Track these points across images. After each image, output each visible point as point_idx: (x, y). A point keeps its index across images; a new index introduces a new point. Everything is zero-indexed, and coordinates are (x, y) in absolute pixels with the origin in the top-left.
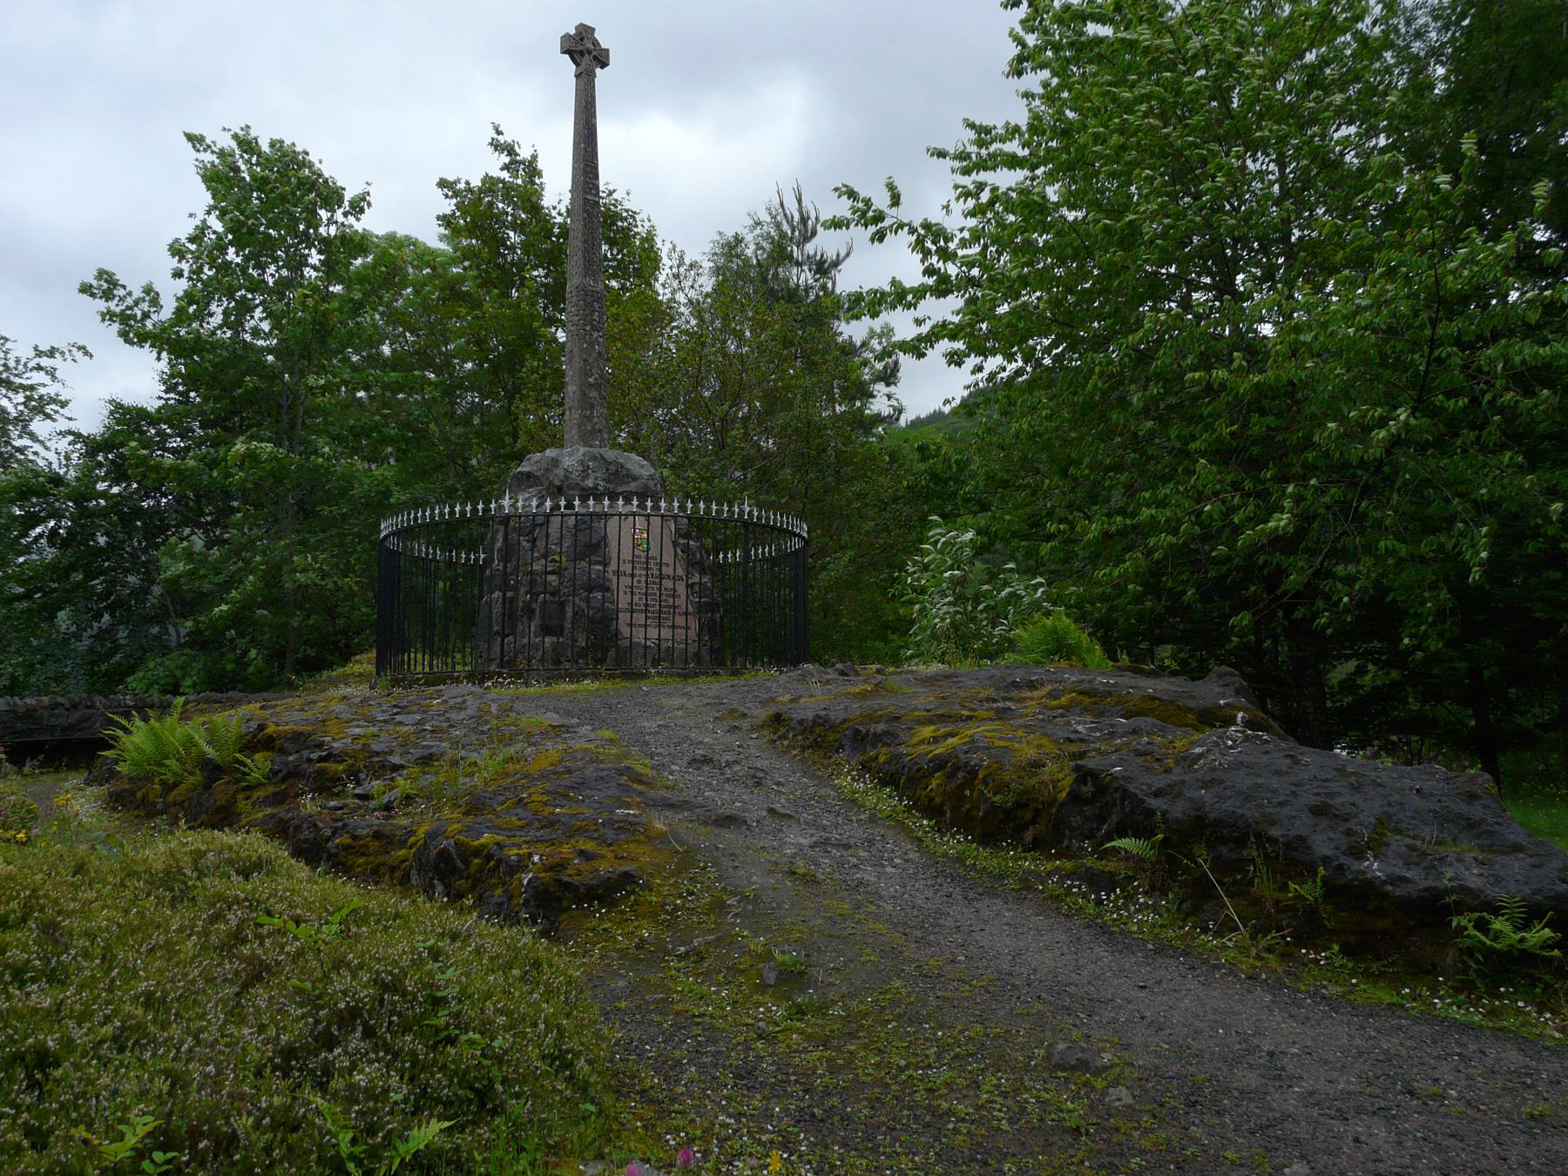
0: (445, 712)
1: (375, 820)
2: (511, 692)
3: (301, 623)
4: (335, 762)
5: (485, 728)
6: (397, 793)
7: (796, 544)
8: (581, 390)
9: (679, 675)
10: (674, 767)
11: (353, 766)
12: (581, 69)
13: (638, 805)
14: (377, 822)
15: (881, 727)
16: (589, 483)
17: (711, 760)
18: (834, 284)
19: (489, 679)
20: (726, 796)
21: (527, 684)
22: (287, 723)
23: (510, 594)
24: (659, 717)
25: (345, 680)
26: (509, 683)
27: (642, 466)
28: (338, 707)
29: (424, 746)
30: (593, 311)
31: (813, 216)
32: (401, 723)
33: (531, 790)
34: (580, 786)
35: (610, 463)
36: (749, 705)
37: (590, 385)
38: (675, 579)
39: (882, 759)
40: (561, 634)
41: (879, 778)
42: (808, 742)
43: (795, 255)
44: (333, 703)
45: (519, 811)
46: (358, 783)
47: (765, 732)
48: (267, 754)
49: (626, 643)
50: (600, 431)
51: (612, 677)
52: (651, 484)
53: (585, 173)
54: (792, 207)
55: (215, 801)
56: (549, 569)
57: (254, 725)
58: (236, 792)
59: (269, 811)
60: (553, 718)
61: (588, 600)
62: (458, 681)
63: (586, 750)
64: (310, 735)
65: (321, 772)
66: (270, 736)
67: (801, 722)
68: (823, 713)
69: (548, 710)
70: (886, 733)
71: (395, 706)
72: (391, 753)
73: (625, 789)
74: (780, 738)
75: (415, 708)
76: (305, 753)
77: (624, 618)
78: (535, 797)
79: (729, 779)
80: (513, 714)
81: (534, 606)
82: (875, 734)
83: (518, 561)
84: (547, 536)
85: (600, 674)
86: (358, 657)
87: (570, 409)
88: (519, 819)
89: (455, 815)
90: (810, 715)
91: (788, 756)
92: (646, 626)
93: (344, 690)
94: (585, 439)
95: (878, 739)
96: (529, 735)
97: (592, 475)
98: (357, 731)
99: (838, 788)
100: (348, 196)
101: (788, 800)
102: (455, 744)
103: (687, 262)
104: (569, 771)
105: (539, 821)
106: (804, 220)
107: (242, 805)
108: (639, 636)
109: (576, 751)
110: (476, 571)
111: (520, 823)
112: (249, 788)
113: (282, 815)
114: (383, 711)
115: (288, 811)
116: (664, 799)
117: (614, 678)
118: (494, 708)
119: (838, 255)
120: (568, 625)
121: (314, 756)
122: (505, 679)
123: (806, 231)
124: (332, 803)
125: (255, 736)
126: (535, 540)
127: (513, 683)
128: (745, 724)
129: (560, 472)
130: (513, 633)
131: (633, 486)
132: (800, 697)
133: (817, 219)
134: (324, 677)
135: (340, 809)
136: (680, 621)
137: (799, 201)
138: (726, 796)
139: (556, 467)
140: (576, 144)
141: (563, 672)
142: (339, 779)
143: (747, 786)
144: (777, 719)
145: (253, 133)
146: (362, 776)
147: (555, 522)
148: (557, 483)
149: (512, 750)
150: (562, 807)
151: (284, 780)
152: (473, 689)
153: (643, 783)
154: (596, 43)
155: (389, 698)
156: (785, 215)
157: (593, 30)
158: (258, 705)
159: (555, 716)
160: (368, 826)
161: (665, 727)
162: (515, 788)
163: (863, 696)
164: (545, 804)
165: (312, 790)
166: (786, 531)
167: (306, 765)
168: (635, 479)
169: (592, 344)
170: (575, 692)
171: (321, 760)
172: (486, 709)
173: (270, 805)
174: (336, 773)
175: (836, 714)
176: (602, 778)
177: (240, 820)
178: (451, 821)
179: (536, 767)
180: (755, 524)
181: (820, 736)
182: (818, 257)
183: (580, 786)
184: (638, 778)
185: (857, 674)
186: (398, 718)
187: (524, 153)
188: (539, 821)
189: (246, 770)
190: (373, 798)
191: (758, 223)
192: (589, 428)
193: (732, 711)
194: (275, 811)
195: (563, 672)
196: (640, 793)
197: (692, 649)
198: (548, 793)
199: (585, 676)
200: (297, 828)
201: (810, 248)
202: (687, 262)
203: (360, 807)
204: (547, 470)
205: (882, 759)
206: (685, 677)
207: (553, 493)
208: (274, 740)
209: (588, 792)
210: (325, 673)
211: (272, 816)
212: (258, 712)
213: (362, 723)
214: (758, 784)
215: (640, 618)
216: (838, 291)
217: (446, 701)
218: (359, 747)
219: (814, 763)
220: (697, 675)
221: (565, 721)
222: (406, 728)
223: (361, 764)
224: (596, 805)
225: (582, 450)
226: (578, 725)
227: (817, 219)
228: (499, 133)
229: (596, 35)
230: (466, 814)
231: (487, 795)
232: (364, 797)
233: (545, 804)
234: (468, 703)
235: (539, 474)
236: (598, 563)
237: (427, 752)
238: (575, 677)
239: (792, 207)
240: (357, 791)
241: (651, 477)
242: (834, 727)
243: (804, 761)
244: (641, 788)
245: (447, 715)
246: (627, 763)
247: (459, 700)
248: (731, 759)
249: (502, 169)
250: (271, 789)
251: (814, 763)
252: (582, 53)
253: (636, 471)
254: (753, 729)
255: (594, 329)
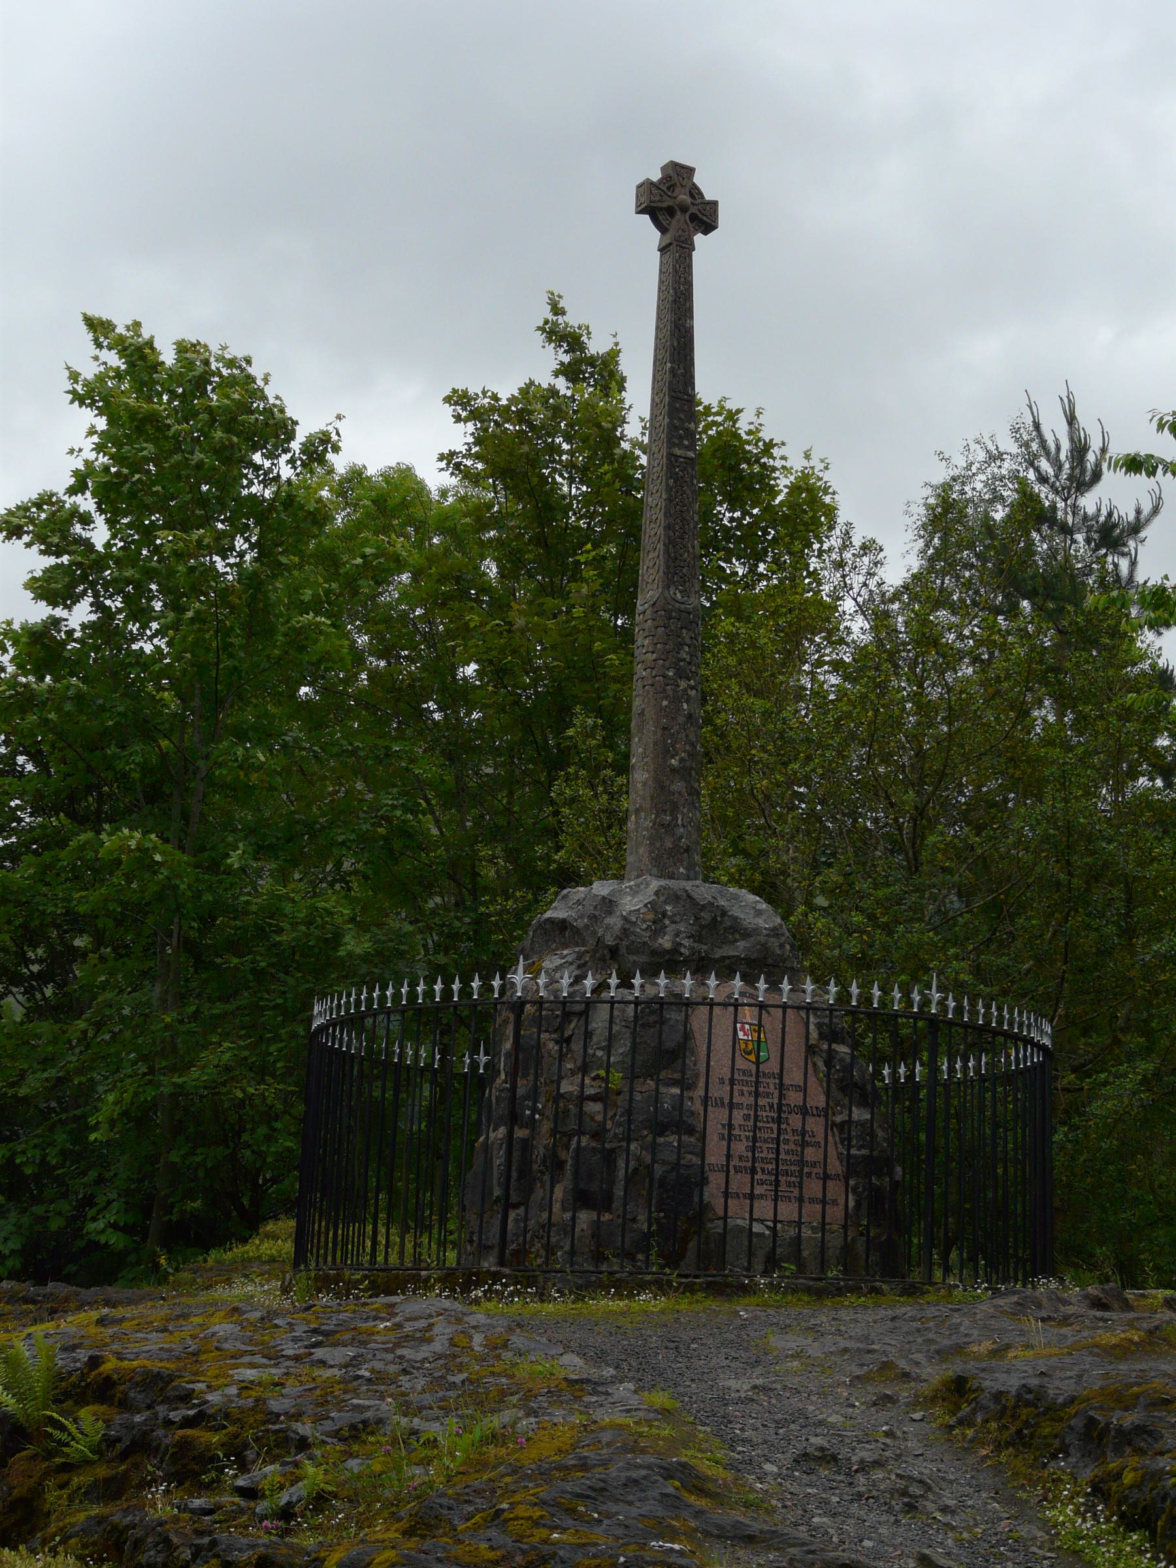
0: (397, 1345)
1: (262, 1537)
2: (513, 1309)
3: (184, 1157)
4: (211, 1429)
5: (458, 1378)
6: (300, 1490)
7: (1017, 1058)
8: (657, 780)
9: (808, 1290)
10: (768, 1467)
11: (236, 1436)
12: (668, 239)
13: (690, 1535)
14: (265, 1539)
15: (1130, 1419)
16: (665, 942)
17: (834, 1458)
18: (1133, 564)
19: (478, 1284)
20: (850, 1527)
21: (542, 1297)
22: (137, 1355)
23: (520, 1133)
24: (759, 1370)
25: (244, 1267)
26: (512, 1294)
27: (759, 913)
28: (223, 1328)
29: (356, 1408)
30: (682, 645)
31: (1095, 444)
32: (323, 1363)
33: (518, 1497)
34: (599, 1493)
35: (703, 908)
36: (917, 1357)
37: (674, 770)
38: (804, 1111)
39: (1128, 1478)
40: (608, 1209)
41: (1122, 1516)
42: (1006, 1435)
43: (1060, 514)
44: (215, 1319)
45: (492, 1533)
46: (243, 1467)
47: (938, 1410)
48: (101, 1408)
49: (717, 1227)
50: (687, 850)
51: (690, 1289)
52: (774, 943)
53: (672, 412)
54: (1055, 428)
55: (11, 1488)
56: (589, 1091)
57: (83, 1355)
58: (46, 1474)
59: (95, 1510)
60: (573, 1364)
61: (653, 1148)
62: (426, 1285)
63: (621, 1427)
64: (171, 1378)
65: (184, 1445)
66: (108, 1378)
67: (998, 1396)
68: (1034, 1382)
69: (567, 1349)
70: (1140, 1430)
71: (315, 1331)
72: (297, 1416)
73: (672, 1502)
74: (961, 1422)
75: (348, 1336)
76: (161, 1410)
77: (716, 1181)
78: (522, 1511)
79: (860, 1495)
80: (507, 1355)
81: (563, 1155)
82: (1120, 1431)
83: (536, 1076)
84: (588, 1035)
85: (669, 1283)
86: (270, 1227)
87: (637, 811)
88: (492, 1548)
89: (391, 1535)
90: (1013, 1383)
91: (971, 1460)
92: (752, 1197)
93: (241, 1289)
94: (662, 865)
95: (1128, 1439)
96: (530, 1395)
97: (671, 928)
98: (250, 1374)
99: (1048, 1526)
100: (301, 435)
101: (959, 1542)
102: (406, 1408)
103: (857, 541)
104: (584, 1466)
105: (524, 1552)
106: (1079, 450)
107: (53, 1497)
108: (739, 1220)
109: (603, 1429)
110: (479, 1082)
111: (492, 1555)
112: (67, 1468)
113: (115, 1519)
114: (295, 1340)
115: (126, 1511)
116: (737, 1524)
117: (693, 1292)
118: (478, 1339)
119: (1138, 512)
120: (619, 1192)
121: (176, 1416)
122: (505, 1286)
123: (1083, 471)
124: (197, 1503)
125: (83, 1377)
126: (568, 1041)
127: (516, 1293)
128: (904, 1393)
129: (614, 921)
130: (525, 1202)
131: (741, 948)
132: (1008, 1347)
133: (1104, 450)
134: (211, 1262)
135: (210, 1512)
136: (813, 1188)
137: (1071, 420)
138: (850, 1527)
139: (610, 913)
140: (658, 362)
141: (604, 1276)
142: (214, 1459)
143: (890, 1511)
144: (959, 1387)
145: (146, 334)
146: (250, 1454)
147: (601, 1016)
148: (609, 941)
149: (495, 1422)
150: (564, 1530)
151: (124, 1456)
152: (447, 1304)
153: (701, 1492)
154: (695, 192)
155: (308, 1315)
156: (1043, 443)
157: (691, 171)
158: (94, 1315)
159: (577, 1361)
160: (253, 1547)
161: (765, 1389)
162: (493, 1491)
163: (1123, 1351)
164: (536, 1523)
165: (168, 1478)
166: (1008, 1035)
167: (160, 1432)
168: (746, 934)
169: (676, 700)
170: (623, 1314)
171: (188, 1423)
172: (465, 1342)
173: (98, 1500)
174: (208, 1447)
175: (1060, 1388)
176: (635, 1481)
177: (47, 1525)
178: (382, 1545)
179: (534, 1454)
180: (951, 1023)
181: (1027, 1424)
182: (1102, 519)
183: (599, 1493)
184: (697, 1484)
185: (1127, 1306)
186: (319, 1353)
187: (597, 346)
188: (524, 1552)
189: (64, 1437)
190: (263, 1497)
191: (995, 457)
192: (669, 844)
193: (886, 1366)
194: (106, 1511)
195: (604, 1276)
196: (698, 1514)
197: (835, 1242)
198: (543, 1503)
199: (643, 1287)
200: (138, 1544)
201: (1088, 502)
202: (857, 541)
203: (242, 1511)
204: (593, 918)
205: (1128, 1478)
206: (819, 1294)
207: (603, 959)
208: (114, 1384)
209: (613, 1508)
210: (214, 1255)
211: (100, 1520)
212: (93, 1330)
213: (259, 1359)
214: (910, 1508)
215: (740, 1183)
216: (1140, 578)
217: (399, 1326)
218: (250, 1402)
219: (1016, 1474)
220: (840, 1292)
221: (593, 1373)
222: (327, 1373)
223: (249, 1434)
224: (620, 1531)
225: (655, 884)
226: (615, 1380)
227: (1104, 450)
228: (557, 310)
229: (697, 179)
230: (408, 1533)
231: (444, 1501)
232: (250, 1493)
233: (536, 1523)
234: (437, 1330)
235: (579, 924)
236: (675, 1083)
237: (357, 1418)
238: (625, 1287)
239: (1055, 428)
240: (240, 1482)
241: (775, 932)
242: (1052, 1411)
243: (997, 1469)
244: (702, 1503)
245: (399, 1352)
246: (685, 1456)
247: (422, 1323)
248: (868, 1456)
249: (556, 374)
250: (102, 1471)
251: (1016, 1474)
252: (671, 211)
253: (748, 919)
254: (914, 1405)
255: (681, 674)
